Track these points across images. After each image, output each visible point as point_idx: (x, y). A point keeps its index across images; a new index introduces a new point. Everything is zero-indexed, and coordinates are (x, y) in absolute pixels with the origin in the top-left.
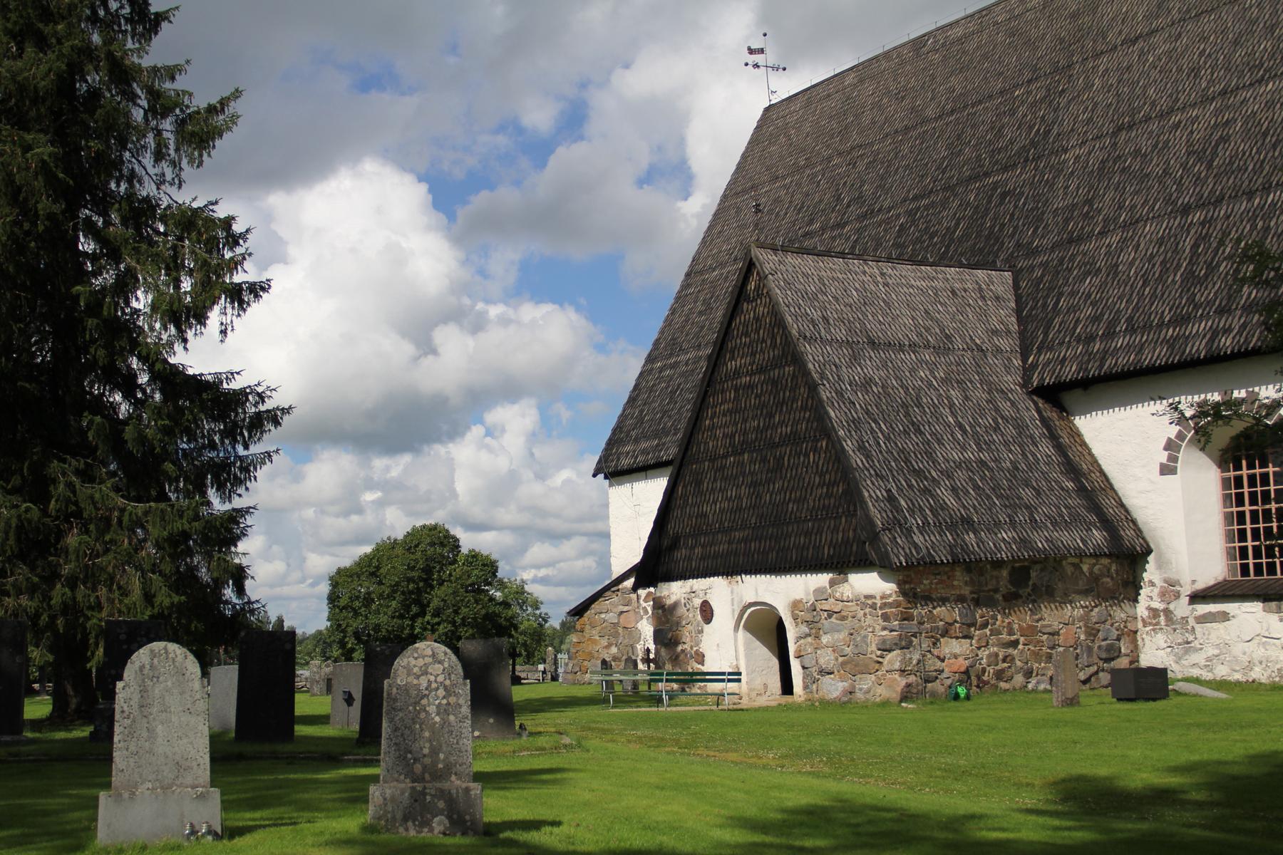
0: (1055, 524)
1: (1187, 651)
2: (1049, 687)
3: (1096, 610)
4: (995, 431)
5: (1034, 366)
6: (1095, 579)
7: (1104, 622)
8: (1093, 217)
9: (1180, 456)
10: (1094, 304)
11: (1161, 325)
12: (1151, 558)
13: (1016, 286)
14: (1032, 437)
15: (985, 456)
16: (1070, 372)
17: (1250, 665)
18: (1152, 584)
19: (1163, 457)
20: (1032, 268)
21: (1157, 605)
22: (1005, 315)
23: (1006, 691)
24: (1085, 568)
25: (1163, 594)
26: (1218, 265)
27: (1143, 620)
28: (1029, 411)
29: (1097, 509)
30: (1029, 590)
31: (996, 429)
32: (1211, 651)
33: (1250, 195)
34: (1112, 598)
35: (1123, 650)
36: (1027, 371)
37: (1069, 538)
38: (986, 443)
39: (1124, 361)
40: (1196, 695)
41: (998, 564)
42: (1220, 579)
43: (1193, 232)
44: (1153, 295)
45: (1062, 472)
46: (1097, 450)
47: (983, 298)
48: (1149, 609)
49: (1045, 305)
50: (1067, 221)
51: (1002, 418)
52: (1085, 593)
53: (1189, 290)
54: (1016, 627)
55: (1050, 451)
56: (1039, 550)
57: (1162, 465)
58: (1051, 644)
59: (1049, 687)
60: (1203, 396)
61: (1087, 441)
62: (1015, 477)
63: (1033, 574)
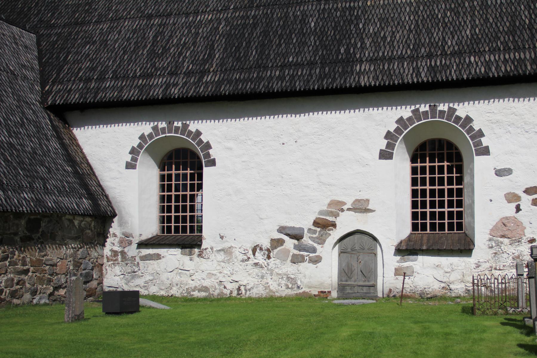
0: (60, 192)
1: (133, 278)
2: (47, 301)
3: (81, 250)
4: (22, 126)
5: (49, 92)
6: (81, 230)
7: (85, 258)
8: (91, 13)
9: (139, 158)
10: (91, 60)
11: (134, 77)
12: (116, 220)
13: (38, 43)
14: (46, 135)
15: (13, 141)
16: (75, 98)
17: (171, 286)
18: (115, 235)
19: (129, 158)
20: (50, 35)
21: (117, 248)
22: (31, 58)
23: (17, 305)
24: (76, 223)
25: (121, 242)
26: (169, 49)
27: (107, 257)
28: (45, 120)
29: (86, 186)
30: (39, 235)
31: (23, 125)
32: (148, 278)
33: (187, 15)
34: (91, 243)
35: (94, 276)
36: (44, 95)
37: (69, 202)
38: (14, 132)
39: (111, 95)
40: (150, 307)
41: (19, 215)
42: (155, 234)
43: (154, 29)
44: (130, 60)
45: (64, 160)
46: (86, 150)
47: (16, 44)
48: (112, 250)
49: (58, 58)
50: (74, 12)
51: (27, 119)
52: (75, 239)
53: (152, 60)
54: (28, 260)
55: (58, 146)
56: (49, 208)
57: (127, 162)
58: (51, 272)
59: (47, 301)
60: (156, 123)
61: (80, 144)
62: (34, 158)
63: (43, 224)
